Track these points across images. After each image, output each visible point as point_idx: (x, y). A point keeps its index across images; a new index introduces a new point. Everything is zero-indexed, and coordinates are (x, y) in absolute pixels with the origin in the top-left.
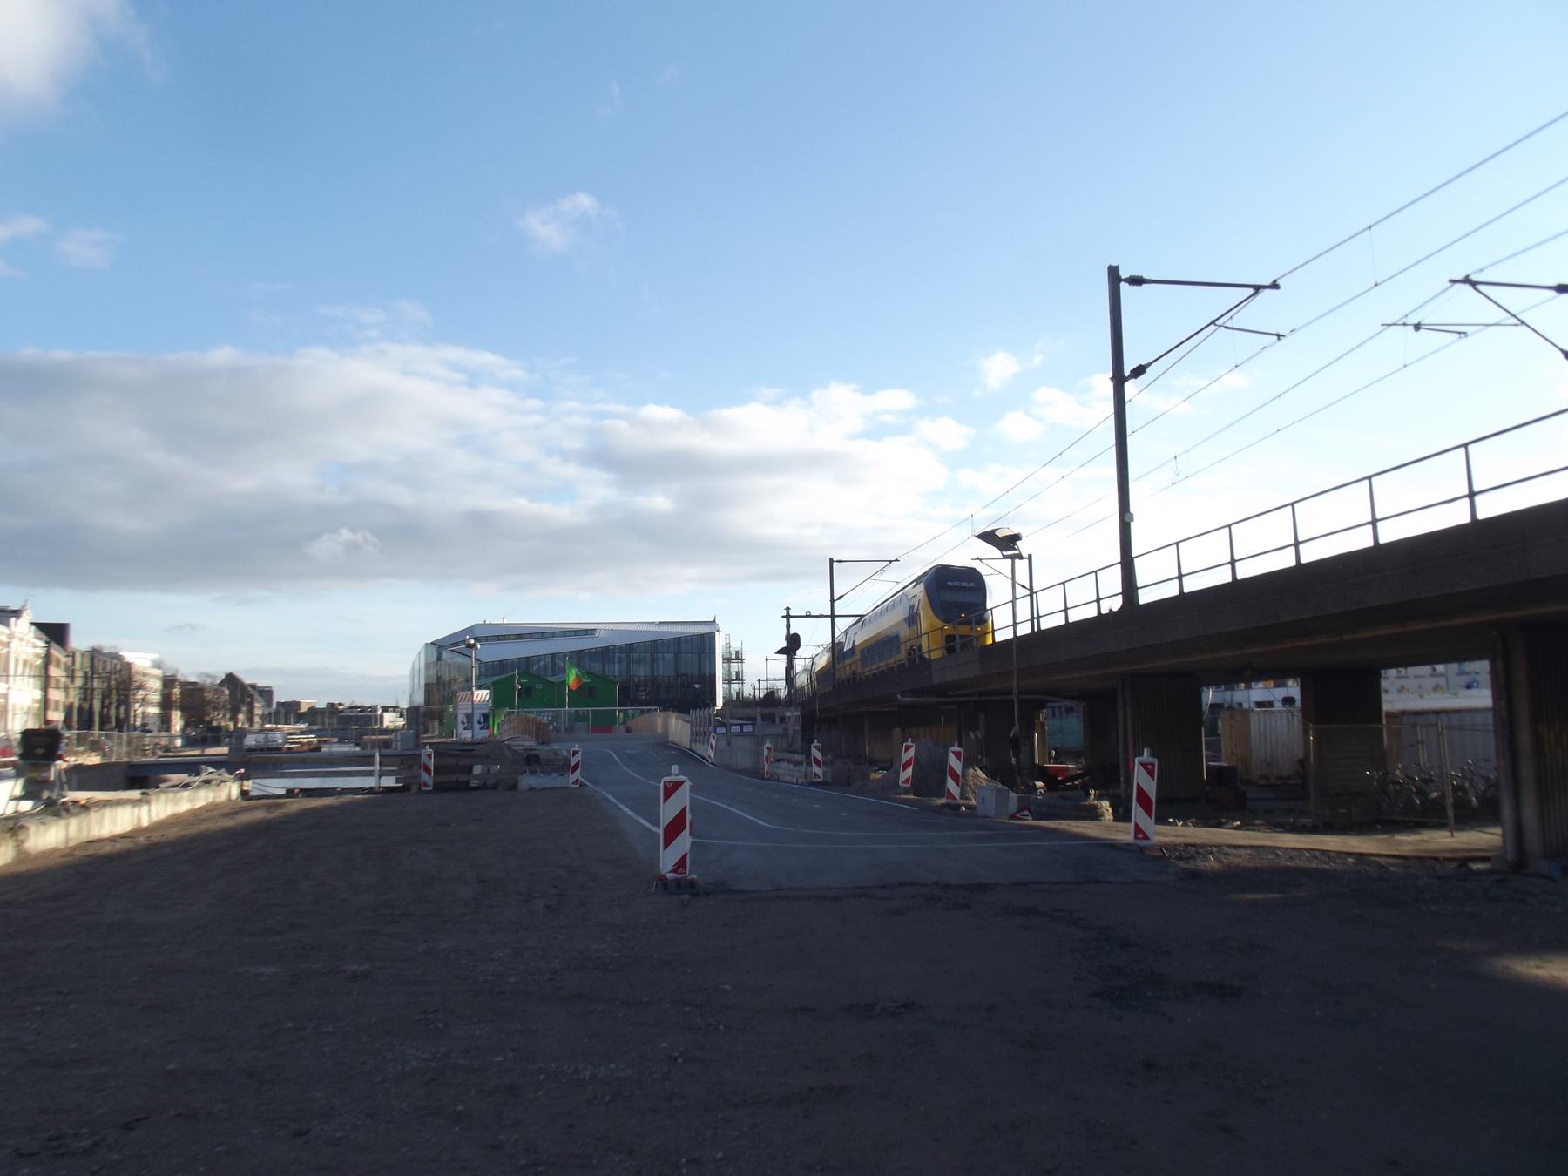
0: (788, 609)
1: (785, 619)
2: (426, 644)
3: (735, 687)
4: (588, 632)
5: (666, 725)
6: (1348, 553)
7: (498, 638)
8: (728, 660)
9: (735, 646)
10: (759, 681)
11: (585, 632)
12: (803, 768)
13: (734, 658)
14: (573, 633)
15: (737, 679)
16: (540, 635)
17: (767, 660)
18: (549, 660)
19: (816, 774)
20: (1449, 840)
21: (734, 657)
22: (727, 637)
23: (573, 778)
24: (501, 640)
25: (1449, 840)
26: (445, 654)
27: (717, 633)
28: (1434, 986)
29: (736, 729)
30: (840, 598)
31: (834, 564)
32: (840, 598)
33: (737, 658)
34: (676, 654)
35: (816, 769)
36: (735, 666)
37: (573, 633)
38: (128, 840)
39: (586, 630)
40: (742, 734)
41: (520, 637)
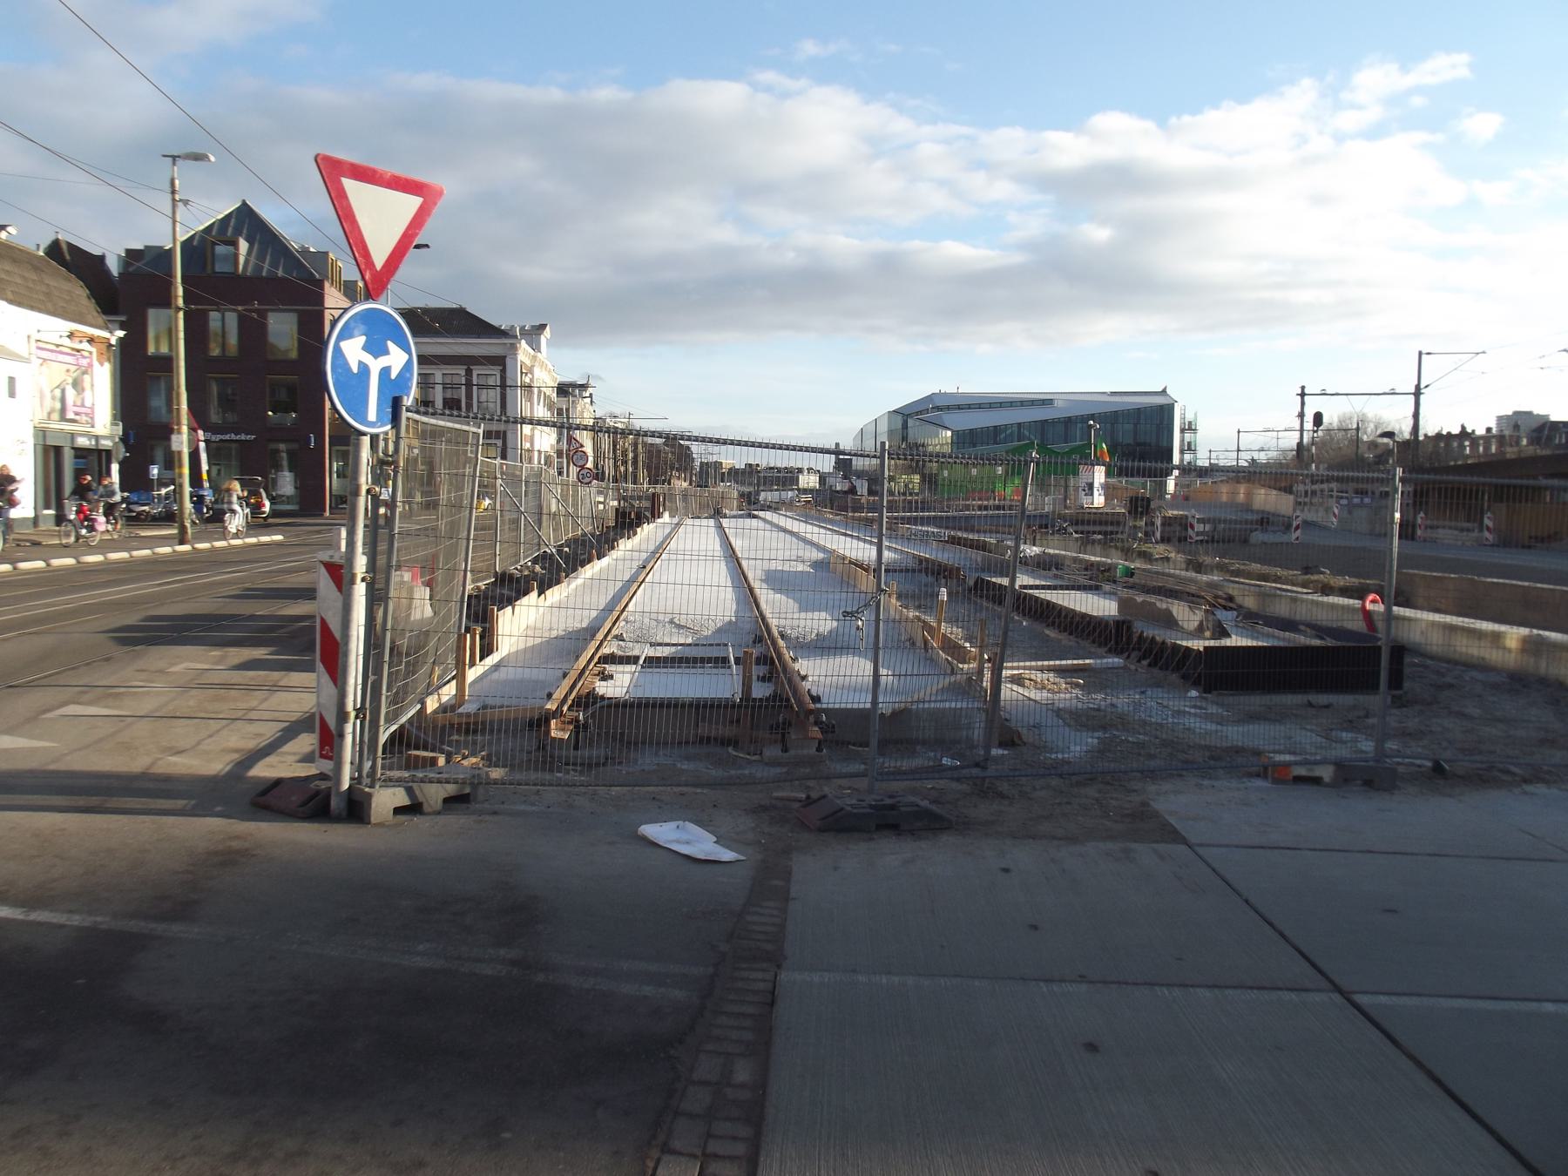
0: (1303, 388)
1: (1299, 397)
2: (889, 412)
3: (1187, 457)
4: (1045, 402)
5: (1249, 495)
6: (436, 308)
7: (969, 407)
8: (1183, 431)
9: (1189, 417)
10: (1210, 451)
11: (999, 405)
12: (1476, 534)
13: (1189, 428)
14: (1031, 403)
15: (1189, 449)
16: (1019, 404)
17: (1239, 432)
18: (1015, 429)
19: (1487, 539)
20: (1156, 632)
21: (1187, 427)
22: (1183, 408)
23: (1294, 536)
24: (962, 409)
25: (1156, 632)
26: (910, 422)
27: (1176, 404)
28: (763, 841)
29: (1356, 501)
30: (1426, 387)
31: (1424, 356)
32: (1426, 387)
33: (1190, 429)
34: (1135, 425)
35: (1487, 534)
36: (1188, 436)
37: (1046, 402)
38: (1257, 588)
39: (1043, 400)
40: (1362, 505)
41: (980, 406)
